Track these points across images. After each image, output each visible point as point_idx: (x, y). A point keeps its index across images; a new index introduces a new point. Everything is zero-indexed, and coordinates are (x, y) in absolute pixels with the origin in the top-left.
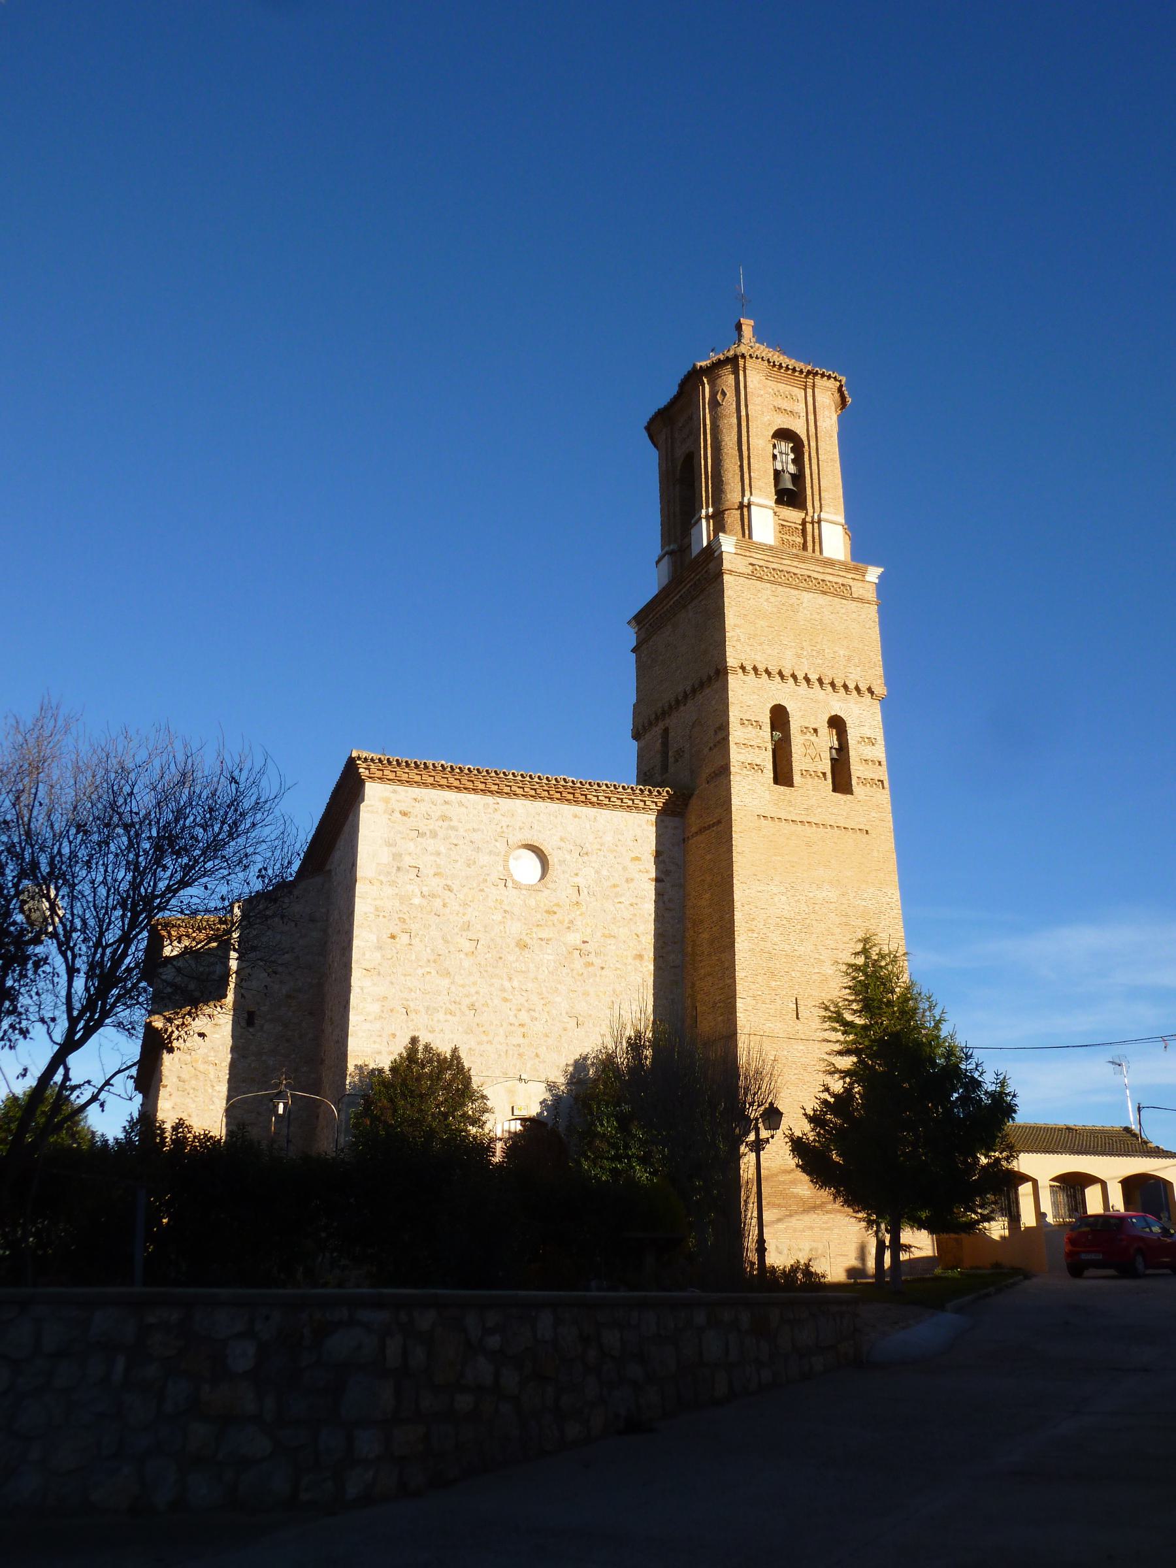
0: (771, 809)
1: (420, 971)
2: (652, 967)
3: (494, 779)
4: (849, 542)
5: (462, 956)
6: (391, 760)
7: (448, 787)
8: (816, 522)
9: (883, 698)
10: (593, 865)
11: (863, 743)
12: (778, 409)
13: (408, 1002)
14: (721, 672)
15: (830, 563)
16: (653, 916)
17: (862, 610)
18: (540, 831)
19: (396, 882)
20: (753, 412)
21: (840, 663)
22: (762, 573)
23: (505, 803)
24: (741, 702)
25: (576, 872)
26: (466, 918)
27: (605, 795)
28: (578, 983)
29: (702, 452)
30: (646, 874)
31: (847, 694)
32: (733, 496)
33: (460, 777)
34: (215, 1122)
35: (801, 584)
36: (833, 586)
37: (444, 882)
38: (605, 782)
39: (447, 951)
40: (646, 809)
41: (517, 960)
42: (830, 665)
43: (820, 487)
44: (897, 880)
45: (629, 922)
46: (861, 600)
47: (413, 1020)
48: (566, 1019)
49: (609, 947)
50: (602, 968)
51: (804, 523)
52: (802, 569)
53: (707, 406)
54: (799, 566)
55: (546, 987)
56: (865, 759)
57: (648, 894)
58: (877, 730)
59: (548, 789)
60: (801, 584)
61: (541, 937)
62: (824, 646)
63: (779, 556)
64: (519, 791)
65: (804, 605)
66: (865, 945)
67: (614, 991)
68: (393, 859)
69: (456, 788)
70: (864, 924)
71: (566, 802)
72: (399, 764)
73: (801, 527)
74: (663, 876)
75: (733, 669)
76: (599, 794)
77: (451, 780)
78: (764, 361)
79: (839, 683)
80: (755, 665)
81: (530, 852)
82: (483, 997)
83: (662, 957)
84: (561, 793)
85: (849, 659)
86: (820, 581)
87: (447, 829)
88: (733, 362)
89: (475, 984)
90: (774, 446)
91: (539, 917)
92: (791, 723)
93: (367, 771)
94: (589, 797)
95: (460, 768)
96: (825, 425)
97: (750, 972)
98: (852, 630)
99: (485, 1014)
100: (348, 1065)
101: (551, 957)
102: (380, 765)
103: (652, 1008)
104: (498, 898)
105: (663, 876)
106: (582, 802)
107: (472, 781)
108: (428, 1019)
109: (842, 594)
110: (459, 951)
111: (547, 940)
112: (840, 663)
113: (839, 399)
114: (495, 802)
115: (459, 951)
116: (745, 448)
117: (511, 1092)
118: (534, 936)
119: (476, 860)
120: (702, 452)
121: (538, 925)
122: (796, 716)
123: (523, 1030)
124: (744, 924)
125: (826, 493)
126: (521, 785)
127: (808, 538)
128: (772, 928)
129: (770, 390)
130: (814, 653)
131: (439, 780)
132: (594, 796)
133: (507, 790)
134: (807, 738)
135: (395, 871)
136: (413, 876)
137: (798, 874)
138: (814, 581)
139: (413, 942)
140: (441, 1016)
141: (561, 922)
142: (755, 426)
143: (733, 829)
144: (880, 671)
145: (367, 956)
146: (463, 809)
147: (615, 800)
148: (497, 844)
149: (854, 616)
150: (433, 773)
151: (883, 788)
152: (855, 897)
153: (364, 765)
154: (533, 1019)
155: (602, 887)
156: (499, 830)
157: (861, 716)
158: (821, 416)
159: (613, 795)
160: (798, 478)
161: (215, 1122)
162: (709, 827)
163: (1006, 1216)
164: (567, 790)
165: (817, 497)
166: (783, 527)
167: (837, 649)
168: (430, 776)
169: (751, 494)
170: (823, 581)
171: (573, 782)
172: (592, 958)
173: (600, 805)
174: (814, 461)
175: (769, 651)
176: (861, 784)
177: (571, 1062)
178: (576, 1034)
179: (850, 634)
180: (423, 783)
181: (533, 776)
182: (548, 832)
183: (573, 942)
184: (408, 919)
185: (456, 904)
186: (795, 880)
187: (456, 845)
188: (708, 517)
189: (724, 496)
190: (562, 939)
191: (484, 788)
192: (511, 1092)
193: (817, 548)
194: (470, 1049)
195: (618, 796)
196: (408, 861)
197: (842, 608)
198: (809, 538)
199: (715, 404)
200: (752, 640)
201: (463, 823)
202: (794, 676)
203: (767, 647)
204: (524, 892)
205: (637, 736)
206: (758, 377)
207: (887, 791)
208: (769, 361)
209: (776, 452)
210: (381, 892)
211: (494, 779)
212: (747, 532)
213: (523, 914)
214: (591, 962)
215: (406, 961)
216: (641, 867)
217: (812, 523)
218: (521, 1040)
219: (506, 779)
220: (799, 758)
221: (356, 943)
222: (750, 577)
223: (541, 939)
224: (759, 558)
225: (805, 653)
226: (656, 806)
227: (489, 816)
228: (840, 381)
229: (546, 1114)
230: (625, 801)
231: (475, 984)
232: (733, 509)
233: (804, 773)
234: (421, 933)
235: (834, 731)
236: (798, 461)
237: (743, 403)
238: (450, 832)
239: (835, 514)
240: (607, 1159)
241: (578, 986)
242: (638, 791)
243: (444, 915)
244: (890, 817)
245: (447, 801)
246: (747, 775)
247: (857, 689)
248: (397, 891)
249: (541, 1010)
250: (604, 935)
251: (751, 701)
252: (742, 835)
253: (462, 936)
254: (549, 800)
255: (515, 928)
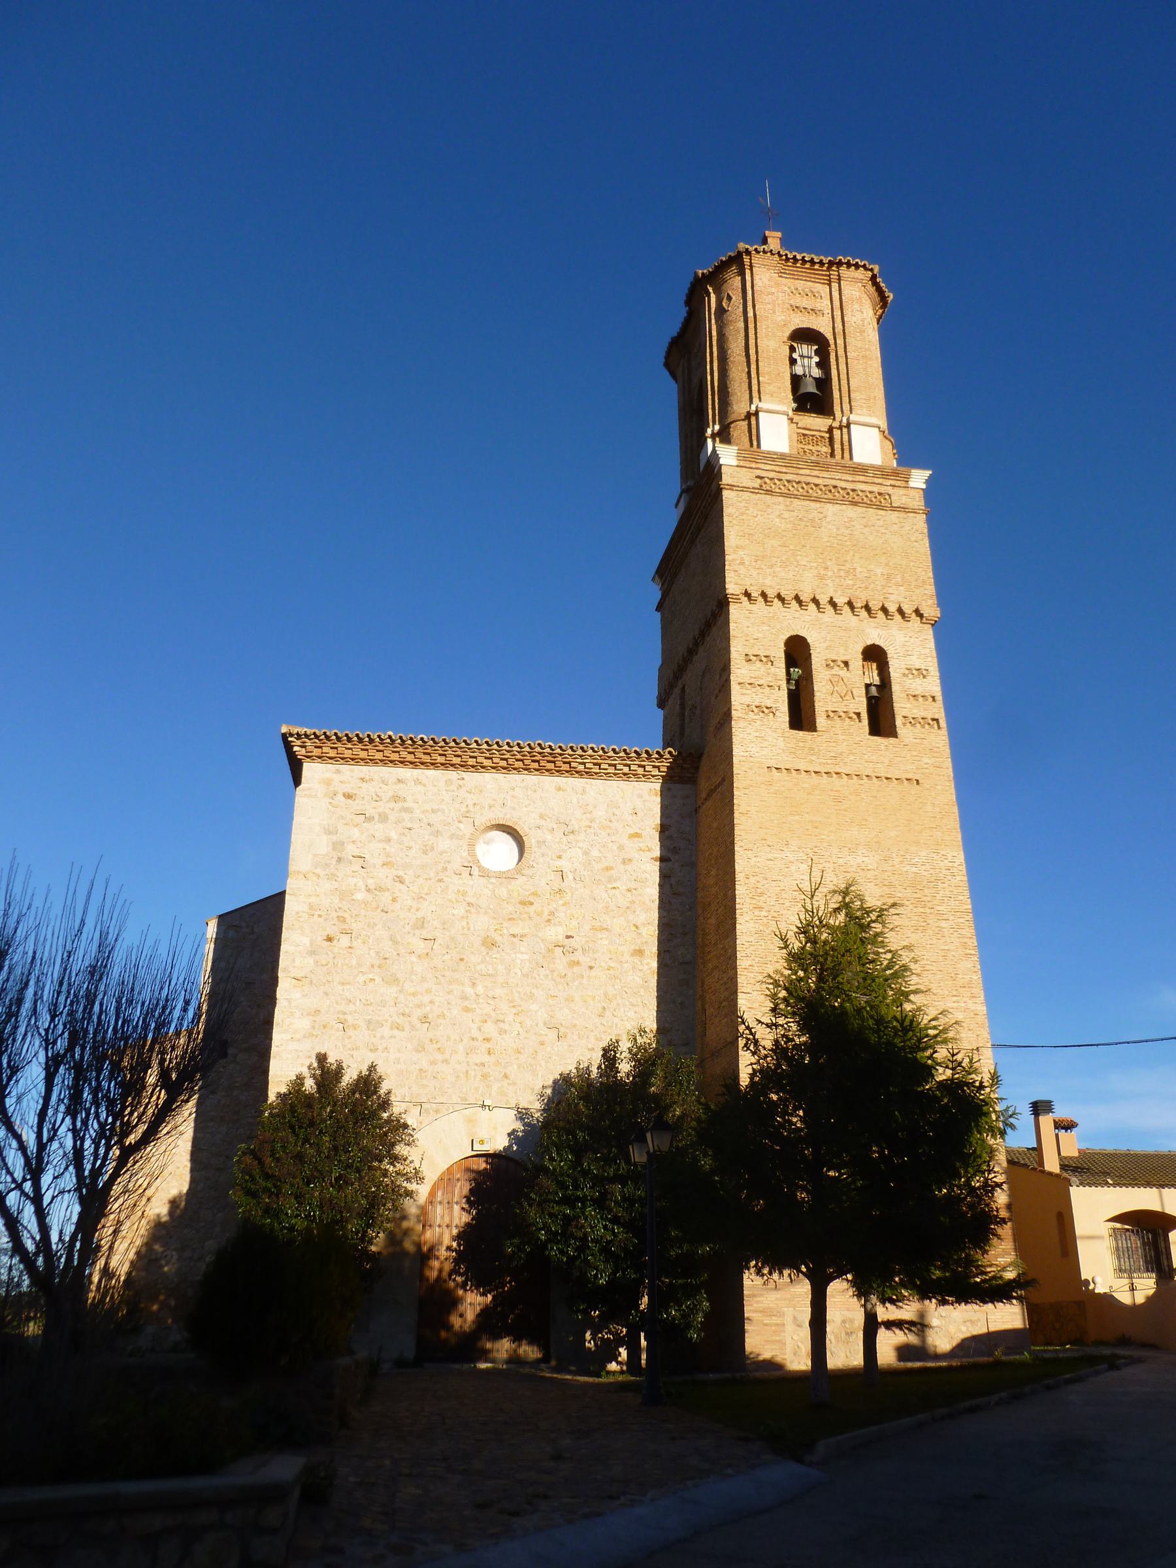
0: (787, 759)
1: (361, 979)
2: (655, 965)
3: (454, 749)
4: (888, 445)
5: (414, 958)
6: (328, 734)
7: (401, 762)
8: (845, 427)
9: (936, 621)
10: (581, 845)
11: (910, 676)
12: (796, 308)
13: (346, 1016)
14: (722, 604)
15: (862, 469)
16: (657, 902)
17: (905, 521)
18: (514, 809)
19: (335, 875)
20: (762, 311)
21: (877, 583)
22: (773, 486)
23: (472, 779)
24: (747, 635)
25: (558, 854)
26: (420, 914)
27: (592, 761)
28: (561, 987)
29: (708, 367)
30: (647, 853)
31: (887, 619)
32: (740, 407)
33: (413, 750)
34: (178, 1168)
35: (825, 496)
36: (867, 496)
37: (395, 873)
38: (590, 746)
39: (395, 954)
40: (646, 776)
41: (482, 962)
42: (863, 586)
43: (849, 387)
44: (960, 839)
45: (625, 911)
46: (903, 509)
47: (350, 1037)
48: (544, 1031)
49: (599, 942)
50: (591, 968)
51: (830, 430)
52: (824, 478)
53: (713, 317)
54: (820, 475)
55: (519, 992)
56: (913, 694)
57: (650, 875)
58: (930, 659)
59: (522, 758)
60: (825, 496)
61: (513, 933)
62: (855, 565)
63: (795, 465)
64: (487, 763)
65: (828, 519)
66: (844, 898)
67: (606, 995)
68: (334, 849)
69: (411, 763)
70: (916, 896)
71: (547, 773)
72: (339, 739)
73: (828, 435)
74: (669, 855)
75: (735, 597)
76: (585, 761)
77: (404, 754)
78: (774, 255)
79: (875, 605)
80: (763, 591)
81: (505, 834)
82: (439, 1006)
83: (668, 951)
84: (538, 761)
85: (889, 578)
86: (849, 491)
87: (400, 811)
88: (737, 261)
89: (429, 991)
90: (792, 349)
91: (511, 908)
92: (812, 656)
93: (304, 749)
94: (573, 764)
95: (411, 739)
96: (854, 319)
97: (757, 959)
98: (892, 545)
99: (441, 1028)
100: (269, 1093)
101: (525, 957)
102: (317, 741)
103: (655, 1014)
104: (461, 889)
105: (669, 855)
106: (567, 772)
107: (429, 754)
108: (369, 1035)
109: (878, 503)
110: (410, 953)
111: (522, 936)
112: (877, 583)
113: (876, 294)
114: (459, 777)
115: (410, 953)
116: (752, 352)
117: (471, 1121)
118: (505, 931)
119: (435, 845)
120: (708, 367)
121: (510, 919)
122: (819, 647)
123: (488, 1045)
124: (748, 900)
125: (858, 394)
126: (488, 755)
127: (836, 446)
128: (788, 904)
129: (786, 289)
130: (842, 573)
131: (388, 755)
132: (580, 763)
133: (472, 762)
134: (835, 673)
135: (334, 863)
136: (357, 867)
137: (823, 837)
138: (842, 492)
139: (354, 944)
140: (386, 1031)
141: (539, 914)
142: (764, 327)
143: (735, 785)
144: (931, 589)
145: (297, 963)
146: (420, 788)
147: (606, 766)
148: (462, 826)
149: (895, 528)
150: (381, 747)
151: (939, 728)
152: (902, 862)
153: (299, 743)
154: (502, 1032)
155: (592, 871)
156: (464, 809)
157: (906, 644)
158: (850, 310)
159: (603, 761)
160: (824, 383)
161: (178, 1168)
162: (716, 787)
163: (1152, 1271)
164: (545, 758)
165: (845, 399)
166: (804, 437)
167: (872, 566)
168: (378, 751)
169: (760, 401)
170: (853, 490)
171: (550, 747)
172: (578, 956)
173: (589, 774)
174: (842, 360)
175: (782, 574)
176: (908, 724)
177: (550, 1082)
178: (556, 1049)
179: (889, 549)
180: (371, 760)
181: (501, 743)
182: (525, 809)
183: (554, 937)
184: (350, 918)
185: (409, 898)
186: (819, 844)
187: (410, 829)
188: (713, 436)
189: (730, 409)
190: (540, 934)
191: (444, 762)
192: (471, 1121)
193: (847, 455)
194: (421, 1070)
195: (610, 762)
196: (351, 849)
197: (878, 520)
198: (837, 446)
199: (721, 311)
200: (759, 562)
201: (420, 802)
202: (815, 601)
203: (779, 569)
204: (493, 880)
205: (661, 704)
206: (767, 275)
207: (944, 731)
208: (780, 256)
209: (795, 356)
210: (316, 887)
211: (454, 749)
212: (755, 443)
213: (491, 907)
214: (576, 960)
215: (345, 967)
216: (641, 845)
217: (840, 428)
218: (486, 1058)
219: (469, 749)
220: (823, 696)
221: (284, 947)
222: (756, 491)
223: (514, 936)
224: (768, 470)
225: (830, 574)
226: (659, 771)
227: (450, 793)
228: (871, 270)
229: (515, 1148)
230: (619, 767)
231: (429, 991)
232: (739, 420)
233: (832, 715)
234: (364, 933)
235: (874, 666)
236: (824, 364)
237: (750, 303)
238: (403, 814)
239: (870, 415)
240: (555, 1202)
241: (559, 991)
242: (633, 755)
243: (393, 911)
244: (948, 763)
245: (400, 778)
246: (754, 721)
247: (900, 611)
248: (336, 885)
249: (513, 1021)
250: (593, 928)
251: (760, 633)
252: (747, 791)
253: (414, 935)
254: (526, 772)
255: (482, 923)
